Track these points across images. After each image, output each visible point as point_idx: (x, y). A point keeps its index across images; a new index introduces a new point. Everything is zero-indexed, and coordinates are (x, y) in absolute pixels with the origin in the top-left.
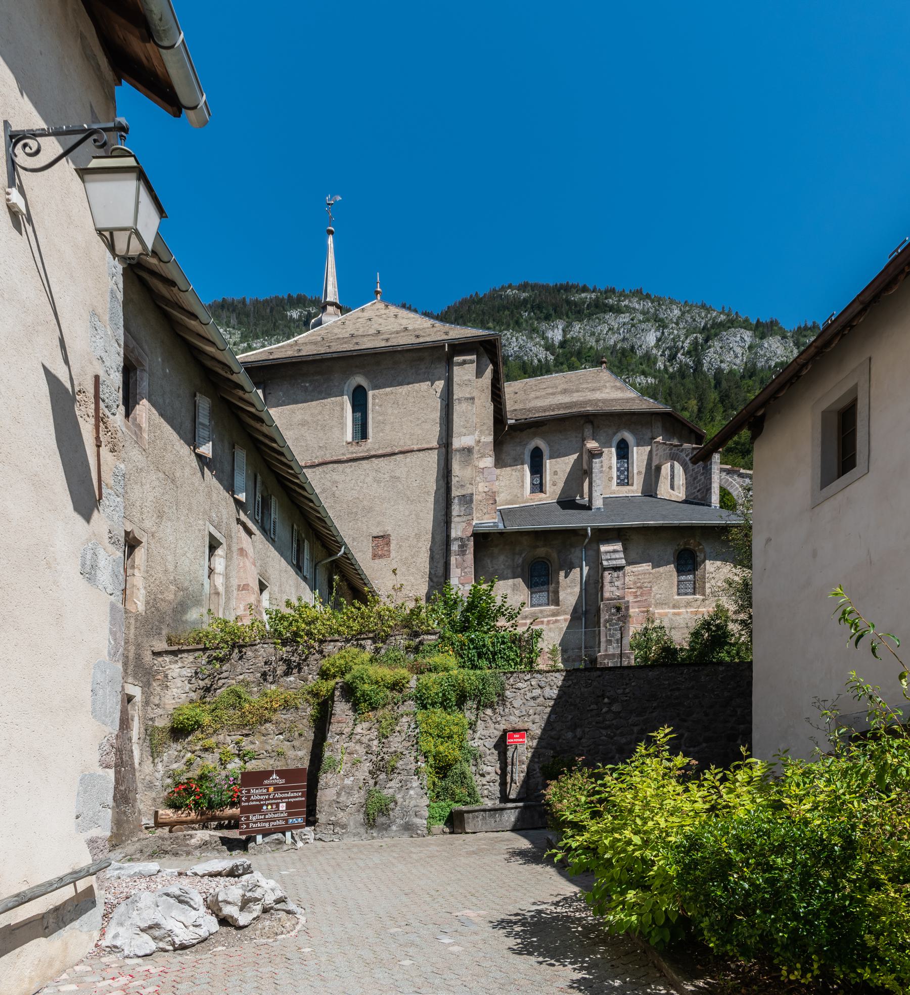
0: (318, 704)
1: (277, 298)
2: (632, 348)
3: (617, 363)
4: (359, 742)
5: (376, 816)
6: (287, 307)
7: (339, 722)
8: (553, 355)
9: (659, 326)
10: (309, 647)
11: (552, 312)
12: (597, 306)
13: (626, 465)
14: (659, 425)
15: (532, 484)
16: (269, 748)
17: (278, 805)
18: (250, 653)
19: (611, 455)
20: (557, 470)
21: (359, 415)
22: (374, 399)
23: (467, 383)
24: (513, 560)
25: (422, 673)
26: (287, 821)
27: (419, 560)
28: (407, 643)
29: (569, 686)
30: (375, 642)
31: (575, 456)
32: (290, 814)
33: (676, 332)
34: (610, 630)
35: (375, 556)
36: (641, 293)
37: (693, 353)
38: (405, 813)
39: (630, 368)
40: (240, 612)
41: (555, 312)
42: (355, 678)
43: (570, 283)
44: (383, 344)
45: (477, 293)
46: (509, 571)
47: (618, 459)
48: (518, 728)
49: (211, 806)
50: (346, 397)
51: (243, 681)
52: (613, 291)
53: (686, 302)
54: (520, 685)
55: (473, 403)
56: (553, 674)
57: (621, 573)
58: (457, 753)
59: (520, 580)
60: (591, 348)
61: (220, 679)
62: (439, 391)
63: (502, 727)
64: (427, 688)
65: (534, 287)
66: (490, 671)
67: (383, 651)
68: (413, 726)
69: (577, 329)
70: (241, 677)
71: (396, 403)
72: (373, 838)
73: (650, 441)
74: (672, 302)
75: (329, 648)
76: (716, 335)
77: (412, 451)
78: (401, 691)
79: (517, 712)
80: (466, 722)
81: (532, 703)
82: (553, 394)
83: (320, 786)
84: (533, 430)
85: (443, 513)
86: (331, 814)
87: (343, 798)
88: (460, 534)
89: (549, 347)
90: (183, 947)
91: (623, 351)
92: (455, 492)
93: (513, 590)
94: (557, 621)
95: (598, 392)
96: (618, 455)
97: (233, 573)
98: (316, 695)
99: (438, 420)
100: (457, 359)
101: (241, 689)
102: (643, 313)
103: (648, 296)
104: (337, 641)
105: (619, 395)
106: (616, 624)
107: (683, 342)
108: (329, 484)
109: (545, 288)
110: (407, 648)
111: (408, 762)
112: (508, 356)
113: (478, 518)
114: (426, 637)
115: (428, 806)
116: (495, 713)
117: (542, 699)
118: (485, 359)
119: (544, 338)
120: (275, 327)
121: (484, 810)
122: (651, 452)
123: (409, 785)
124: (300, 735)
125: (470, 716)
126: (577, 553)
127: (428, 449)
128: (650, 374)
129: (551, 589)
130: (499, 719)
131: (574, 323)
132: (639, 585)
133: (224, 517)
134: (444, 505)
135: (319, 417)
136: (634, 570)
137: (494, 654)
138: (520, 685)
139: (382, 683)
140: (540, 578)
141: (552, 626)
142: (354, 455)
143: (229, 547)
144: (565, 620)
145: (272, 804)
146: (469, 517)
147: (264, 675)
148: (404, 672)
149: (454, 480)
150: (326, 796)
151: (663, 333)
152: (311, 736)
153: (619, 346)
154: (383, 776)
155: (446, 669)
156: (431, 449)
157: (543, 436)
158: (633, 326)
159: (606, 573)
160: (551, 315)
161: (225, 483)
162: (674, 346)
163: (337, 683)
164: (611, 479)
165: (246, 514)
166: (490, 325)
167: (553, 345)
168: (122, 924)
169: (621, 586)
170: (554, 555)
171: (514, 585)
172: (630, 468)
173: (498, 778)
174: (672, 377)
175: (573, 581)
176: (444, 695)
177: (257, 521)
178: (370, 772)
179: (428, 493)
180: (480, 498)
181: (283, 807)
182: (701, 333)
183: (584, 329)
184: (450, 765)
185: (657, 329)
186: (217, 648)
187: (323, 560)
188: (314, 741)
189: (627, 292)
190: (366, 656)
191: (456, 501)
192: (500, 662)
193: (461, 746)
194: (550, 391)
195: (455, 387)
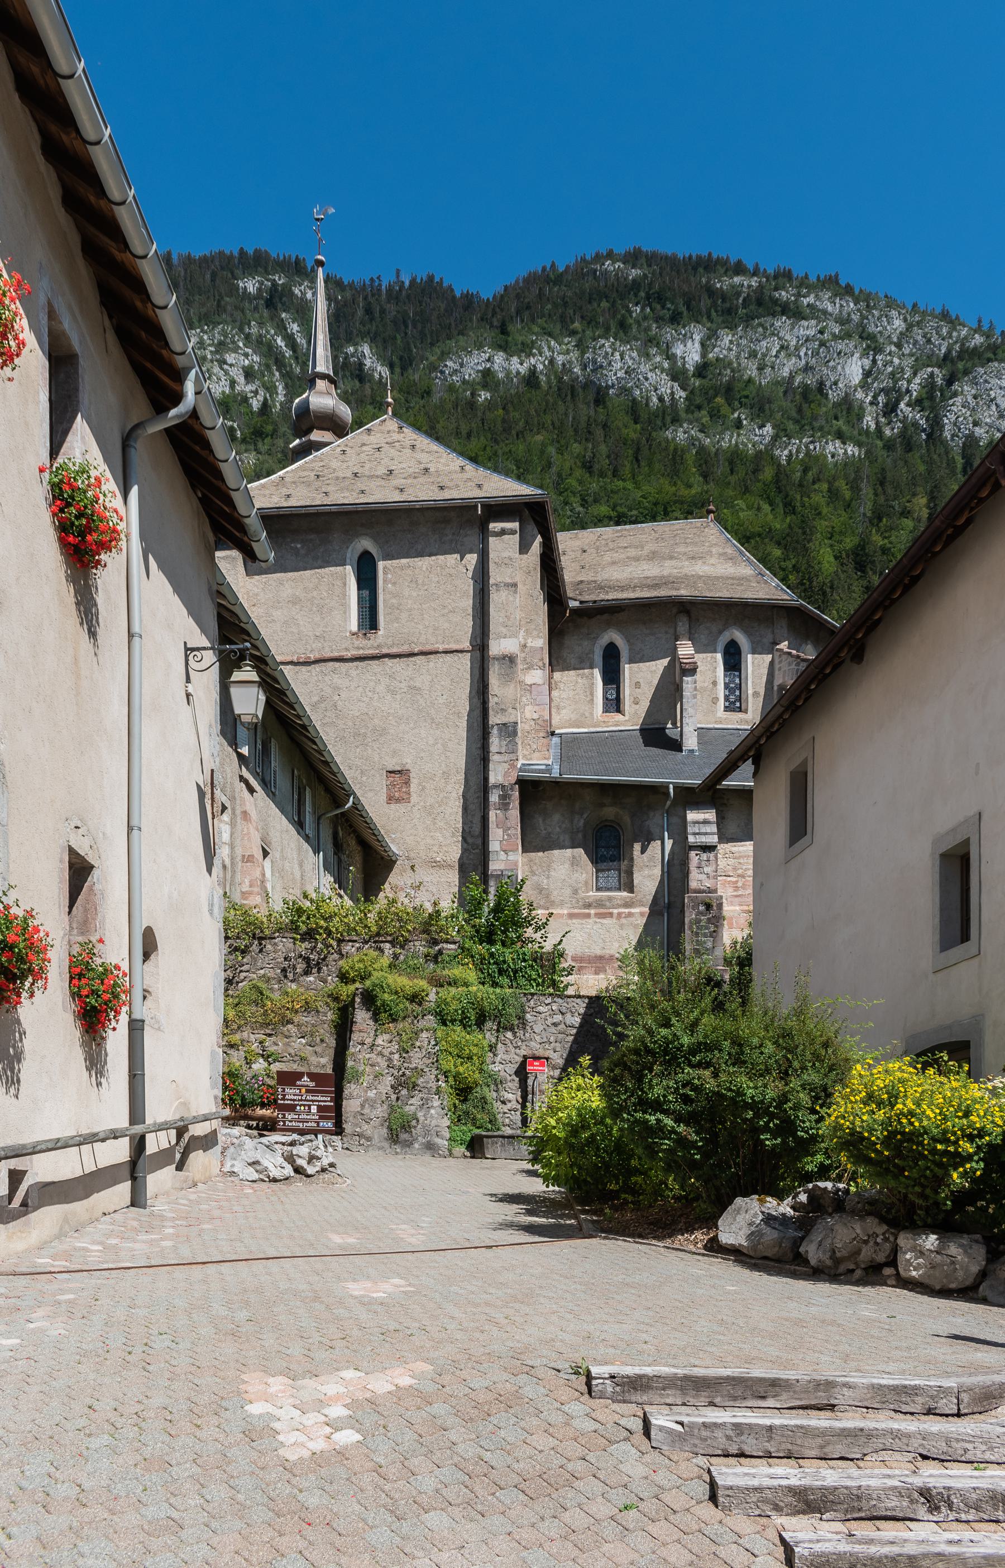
0: (339, 1009)
1: (221, 253)
2: (821, 384)
3: (794, 413)
4: (380, 1054)
5: (399, 1132)
6: (238, 272)
7: (360, 1031)
8: (685, 390)
9: (868, 347)
10: (328, 946)
11: (683, 309)
12: (760, 303)
13: (737, 681)
14: (784, 623)
15: (606, 698)
16: (292, 1052)
17: (309, 1106)
18: (269, 947)
19: (711, 667)
20: (642, 679)
21: (366, 593)
22: (385, 573)
23: (507, 563)
24: (572, 822)
25: (442, 986)
26: (318, 1123)
27: (449, 811)
28: (426, 950)
29: (591, 1015)
30: (394, 947)
31: (665, 662)
32: (321, 1118)
33: (896, 361)
34: (697, 934)
35: (390, 799)
36: (837, 283)
37: (926, 403)
38: (427, 1132)
39: (816, 424)
40: (245, 888)
41: (688, 309)
42: (375, 985)
43: (715, 256)
44: (397, 497)
45: (553, 265)
46: (567, 837)
47: (726, 670)
48: (538, 1055)
49: (243, 1105)
50: (349, 568)
51: (264, 976)
52: (788, 275)
53: (915, 305)
54: (541, 1009)
55: (515, 592)
56: (575, 1000)
57: (712, 855)
58: (477, 1075)
59: (581, 850)
60: (750, 380)
61: (241, 971)
62: (471, 568)
63: (523, 1052)
64: (447, 1004)
65: (651, 258)
66: (511, 990)
67: (402, 957)
68: (433, 1043)
69: (727, 344)
70: (262, 972)
71: (414, 581)
72: (397, 1153)
73: (770, 648)
74: (891, 303)
75: (347, 948)
76: (966, 372)
77: (437, 652)
78: (420, 1004)
79: (538, 1038)
80: (485, 1043)
81: (553, 1029)
82: (637, 559)
83: (344, 1096)
84: (606, 616)
85: (479, 745)
86: (356, 1125)
87: (367, 1111)
88: (500, 779)
89: (677, 375)
90: (275, 1180)
91: (806, 390)
92: (494, 719)
93: (572, 864)
94: (630, 915)
95: (700, 562)
96: (725, 664)
97: (238, 842)
98: (336, 999)
99: (470, 611)
100: (495, 526)
101: (262, 985)
102: (842, 321)
103: (849, 290)
104: (355, 941)
105: (727, 569)
106: (707, 928)
107: (909, 382)
108: (329, 690)
109: (671, 263)
110: (426, 956)
111: (429, 1079)
112: (608, 387)
113: (525, 757)
114: (445, 945)
115: (448, 1127)
116: (515, 1037)
117: (562, 1026)
118: (532, 528)
119: (671, 357)
120: (220, 308)
121: (503, 1137)
122: (772, 663)
123: (430, 1104)
124: (322, 1041)
125: (490, 1037)
126: (656, 819)
127: (457, 651)
128: (851, 439)
129: (623, 867)
130: (520, 1044)
131: (721, 332)
132: (740, 872)
133: (229, 776)
134: (480, 733)
135: (315, 593)
136: (734, 849)
137: (515, 972)
138: (541, 1009)
139: (401, 994)
140: (608, 850)
141: (624, 921)
142: (361, 652)
143: (233, 810)
144: (642, 914)
145: (304, 1105)
146: (512, 756)
147: (284, 970)
148: (423, 984)
149: (492, 701)
150: (351, 1106)
151: (874, 361)
152: (333, 1043)
153: (798, 380)
154: (404, 1092)
155: (466, 984)
156: (461, 651)
157: (619, 627)
158: (822, 344)
159: (693, 854)
160: (681, 314)
161: (229, 735)
162: (894, 389)
163: (357, 989)
164: (715, 700)
165: (247, 769)
166: (577, 325)
167: (685, 371)
168: (235, 1159)
169: (712, 874)
170: (627, 819)
171: (574, 857)
172: (743, 685)
173: (519, 1107)
174: (889, 445)
175: (652, 859)
176: (463, 1012)
177: (258, 774)
178: (392, 1087)
179: (458, 714)
180: (527, 727)
181: (314, 1109)
182: (939, 367)
183: (738, 345)
184: (471, 1088)
185: (864, 354)
186: (238, 938)
187: (328, 812)
188: (336, 1049)
189: (813, 279)
190: (385, 961)
191: (495, 731)
192: (522, 982)
193: (481, 1069)
194: (632, 552)
195: (492, 566)
